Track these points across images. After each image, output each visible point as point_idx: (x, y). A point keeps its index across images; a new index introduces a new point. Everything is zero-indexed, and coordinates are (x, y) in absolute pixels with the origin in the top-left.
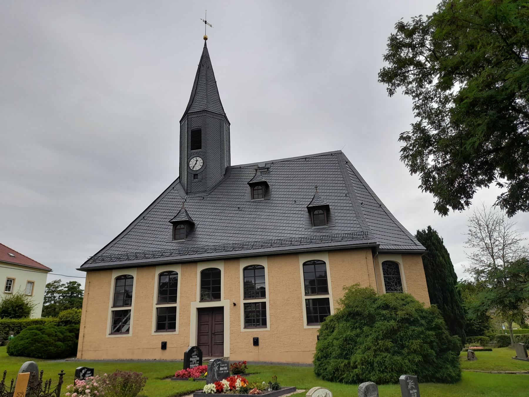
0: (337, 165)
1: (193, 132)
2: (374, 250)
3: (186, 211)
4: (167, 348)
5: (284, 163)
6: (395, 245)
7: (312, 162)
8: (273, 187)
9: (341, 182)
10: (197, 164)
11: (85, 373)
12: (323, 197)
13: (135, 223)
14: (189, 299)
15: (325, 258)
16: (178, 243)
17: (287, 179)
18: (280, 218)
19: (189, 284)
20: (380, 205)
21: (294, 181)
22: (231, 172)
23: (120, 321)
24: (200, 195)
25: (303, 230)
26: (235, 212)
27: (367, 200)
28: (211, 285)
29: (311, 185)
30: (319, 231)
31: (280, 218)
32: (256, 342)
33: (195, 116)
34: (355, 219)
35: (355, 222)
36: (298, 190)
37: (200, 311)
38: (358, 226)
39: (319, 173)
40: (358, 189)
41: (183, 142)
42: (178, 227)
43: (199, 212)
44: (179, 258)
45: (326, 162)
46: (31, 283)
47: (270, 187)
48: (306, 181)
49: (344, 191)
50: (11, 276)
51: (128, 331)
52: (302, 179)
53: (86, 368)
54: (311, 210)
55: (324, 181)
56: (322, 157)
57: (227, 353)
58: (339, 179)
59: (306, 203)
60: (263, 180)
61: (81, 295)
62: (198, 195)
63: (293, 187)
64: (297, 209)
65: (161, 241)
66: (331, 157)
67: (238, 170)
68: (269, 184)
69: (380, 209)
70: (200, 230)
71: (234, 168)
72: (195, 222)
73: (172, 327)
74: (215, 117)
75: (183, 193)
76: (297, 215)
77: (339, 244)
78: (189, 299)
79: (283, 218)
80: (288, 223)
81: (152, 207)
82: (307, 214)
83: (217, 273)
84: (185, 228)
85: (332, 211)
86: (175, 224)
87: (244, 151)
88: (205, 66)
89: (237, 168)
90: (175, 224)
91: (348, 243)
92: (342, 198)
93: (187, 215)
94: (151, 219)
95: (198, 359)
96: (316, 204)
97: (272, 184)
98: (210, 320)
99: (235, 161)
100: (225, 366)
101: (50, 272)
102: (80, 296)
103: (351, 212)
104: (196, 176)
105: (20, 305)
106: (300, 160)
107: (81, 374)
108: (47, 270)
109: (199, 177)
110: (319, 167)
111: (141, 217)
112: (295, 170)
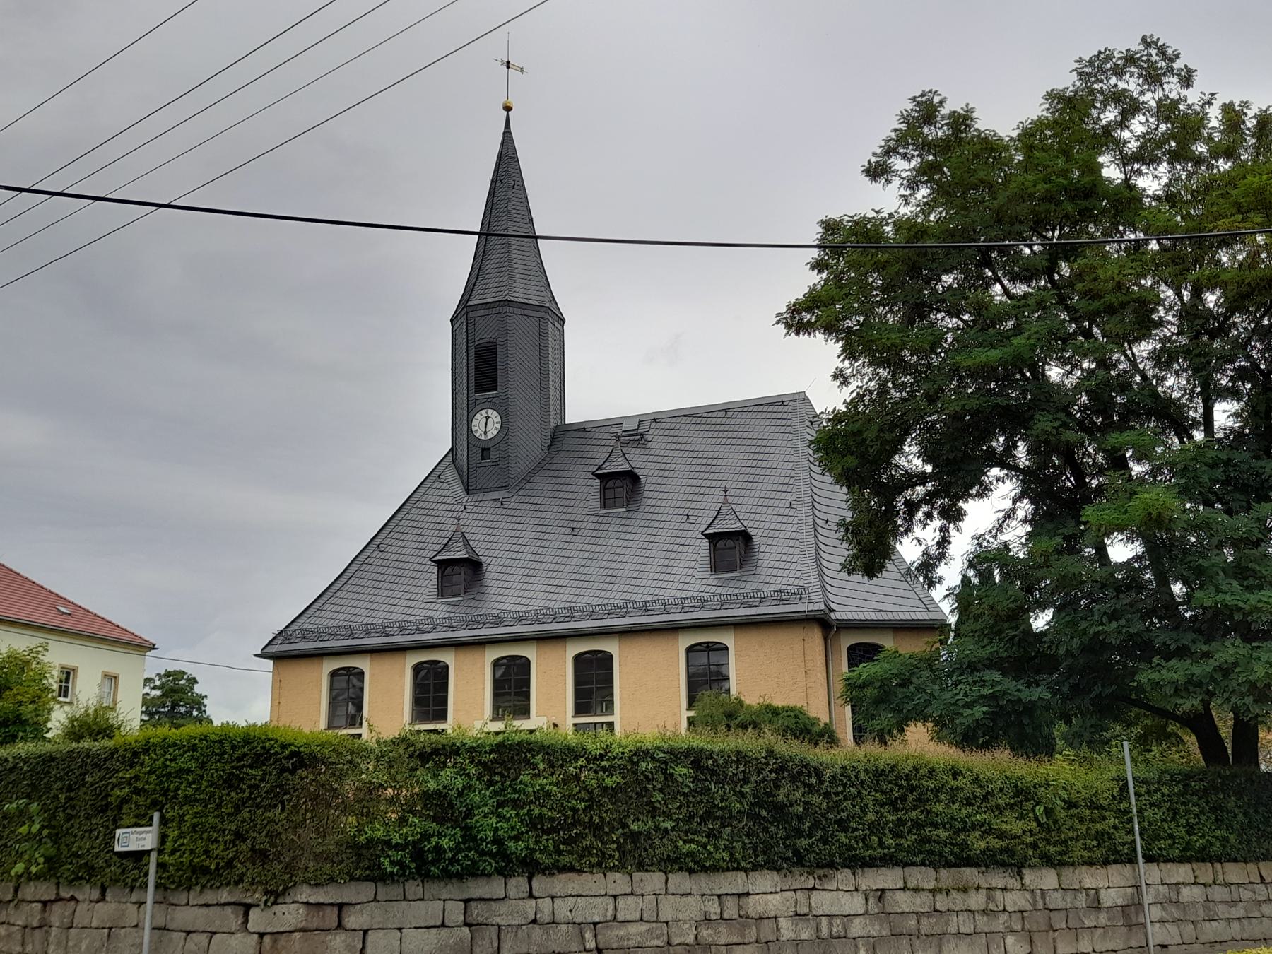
2: (825, 624)
5: (679, 420)
6: (875, 611)
10: (487, 424)
13: (361, 559)
15: (728, 639)
16: (449, 604)
17: (680, 460)
22: (564, 439)
24: (496, 495)
26: (564, 538)
30: (724, 583)
33: (482, 312)
41: (458, 370)
43: (493, 533)
44: (450, 634)
46: (112, 678)
50: (69, 663)
61: (199, 709)
63: (690, 482)
65: (418, 604)
70: (493, 576)
72: (483, 559)
75: (458, 489)
77: (753, 611)
79: (659, 554)
80: (675, 573)
81: (395, 521)
84: (460, 574)
85: (756, 541)
86: (444, 565)
87: (604, 379)
88: (507, 160)
89: (578, 430)
90: (444, 565)
92: (781, 511)
96: (720, 528)
101: (152, 653)
102: (195, 713)
104: (485, 452)
105: (105, 730)
106: (715, 414)
108: (145, 647)
109: (493, 454)
111: (373, 546)
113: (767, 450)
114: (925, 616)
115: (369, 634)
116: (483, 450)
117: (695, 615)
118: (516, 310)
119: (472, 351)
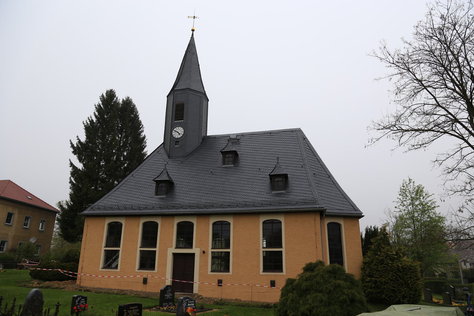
0: (296, 140)
1: (176, 105)
2: (322, 213)
3: (167, 172)
4: (148, 284)
6: (339, 209)
7: (276, 137)
8: (242, 155)
9: (299, 155)
11: (80, 300)
12: (283, 167)
14: (167, 246)
18: (246, 183)
19: (167, 234)
20: (329, 176)
21: (260, 152)
23: (111, 259)
25: (265, 194)
27: (319, 171)
28: (185, 235)
29: (274, 155)
31: (246, 183)
32: (220, 282)
33: (180, 92)
34: (308, 187)
35: (308, 189)
36: (262, 160)
37: (175, 255)
38: (310, 193)
39: (281, 146)
40: (313, 161)
42: (160, 185)
45: (288, 137)
47: (240, 156)
48: (270, 153)
49: (301, 163)
51: (116, 267)
52: (266, 150)
53: (81, 296)
54: (272, 177)
55: (284, 154)
56: (284, 133)
57: (196, 290)
58: (297, 152)
59: (269, 171)
60: (234, 149)
62: (178, 159)
64: (261, 176)
66: (292, 133)
67: (213, 139)
68: (238, 153)
69: (329, 179)
70: (178, 189)
71: (210, 137)
72: (174, 182)
73: (152, 267)
74: (196, 94)
75: (166, 157)
76: (260, 181)
77: (294, 207)
78: (167, 246)
80: (256, 191)
82: (268, 181)
83: (191, 225)
85: (290, 179)
86: (158, 182)
87: (221, 122)
89: (213, 138)
90: (158, 182)
91: (301, 207)
92: (298, 169)
93: (168, 175)
94: (138, 177)
95: (171, 295)
96: (277, 172)
97: (241, 153)
98: (183, 265)
99: (210, 133)
100: (193, 303)
103: (305, 181)
107: (77, 301)
110: (281, 142)
112: (261, 143)
113: (289, 147)
114: (354, 212)
115: (126, 208)
116: (176, 142)
117: (268, 208)
118: (192, 92)
119: (175, 106)
